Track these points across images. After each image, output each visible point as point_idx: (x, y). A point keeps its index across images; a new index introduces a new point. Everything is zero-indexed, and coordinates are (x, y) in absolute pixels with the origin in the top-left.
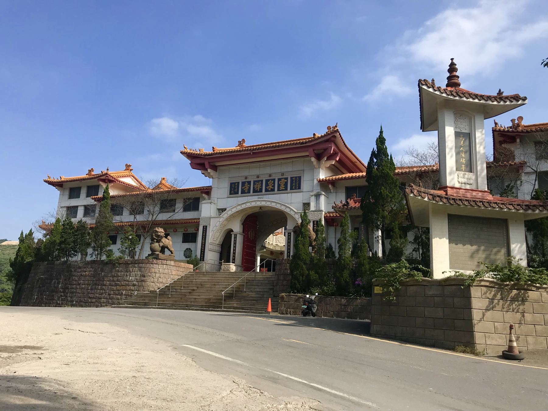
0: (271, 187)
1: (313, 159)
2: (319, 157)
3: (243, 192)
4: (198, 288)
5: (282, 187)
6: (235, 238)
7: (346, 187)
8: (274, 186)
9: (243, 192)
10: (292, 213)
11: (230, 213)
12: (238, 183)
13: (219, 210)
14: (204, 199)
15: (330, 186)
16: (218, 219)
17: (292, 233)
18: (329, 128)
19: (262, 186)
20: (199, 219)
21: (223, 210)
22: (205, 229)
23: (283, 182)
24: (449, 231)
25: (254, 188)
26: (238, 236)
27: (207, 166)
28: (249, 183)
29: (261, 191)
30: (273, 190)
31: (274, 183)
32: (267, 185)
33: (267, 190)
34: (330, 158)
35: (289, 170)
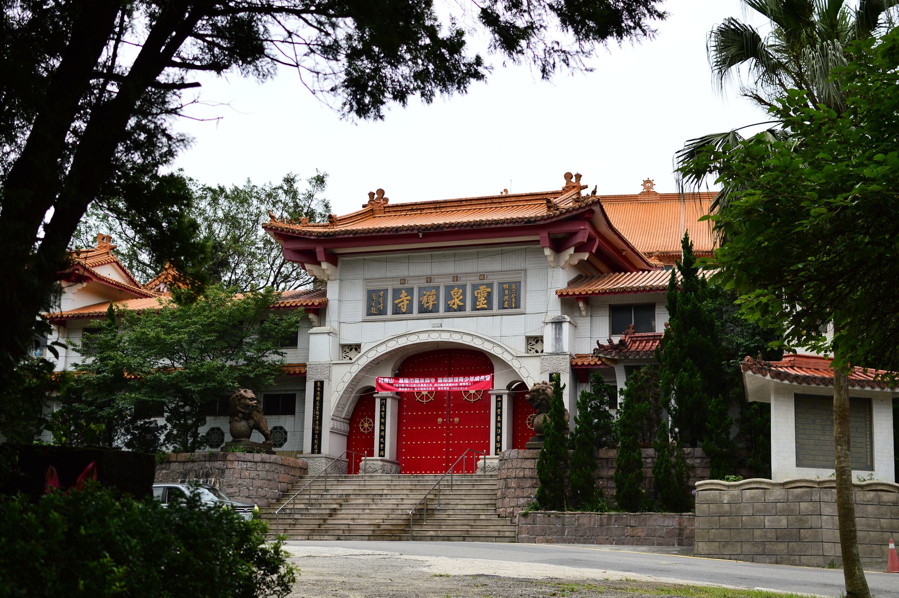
0: (457, 301)
1: (547, 252)
4: (341, 505)
5: (482, 303)
6: (384, 405)
7: (610, 306)
8: (463, 300)
9: (397, 311)
10: (506, 357)
11: (373, 355)
13: (343, 346)
15: (581, 305)
17: (505, 399)
18: (573, 181)
19: (438, 299)
21: (357, 347)
22: (319, 387)
23: (483, 291)
24: (796, 420)
25: (420, 302)
26: (389, 401)
27: (320, 256)
28: (410, 291)
29: (435, 309)
30: (461, 308)
31: (464, 294)
32: (448, 297)
33: (449, 309)
34: (579, 249)
35: (496, 267)
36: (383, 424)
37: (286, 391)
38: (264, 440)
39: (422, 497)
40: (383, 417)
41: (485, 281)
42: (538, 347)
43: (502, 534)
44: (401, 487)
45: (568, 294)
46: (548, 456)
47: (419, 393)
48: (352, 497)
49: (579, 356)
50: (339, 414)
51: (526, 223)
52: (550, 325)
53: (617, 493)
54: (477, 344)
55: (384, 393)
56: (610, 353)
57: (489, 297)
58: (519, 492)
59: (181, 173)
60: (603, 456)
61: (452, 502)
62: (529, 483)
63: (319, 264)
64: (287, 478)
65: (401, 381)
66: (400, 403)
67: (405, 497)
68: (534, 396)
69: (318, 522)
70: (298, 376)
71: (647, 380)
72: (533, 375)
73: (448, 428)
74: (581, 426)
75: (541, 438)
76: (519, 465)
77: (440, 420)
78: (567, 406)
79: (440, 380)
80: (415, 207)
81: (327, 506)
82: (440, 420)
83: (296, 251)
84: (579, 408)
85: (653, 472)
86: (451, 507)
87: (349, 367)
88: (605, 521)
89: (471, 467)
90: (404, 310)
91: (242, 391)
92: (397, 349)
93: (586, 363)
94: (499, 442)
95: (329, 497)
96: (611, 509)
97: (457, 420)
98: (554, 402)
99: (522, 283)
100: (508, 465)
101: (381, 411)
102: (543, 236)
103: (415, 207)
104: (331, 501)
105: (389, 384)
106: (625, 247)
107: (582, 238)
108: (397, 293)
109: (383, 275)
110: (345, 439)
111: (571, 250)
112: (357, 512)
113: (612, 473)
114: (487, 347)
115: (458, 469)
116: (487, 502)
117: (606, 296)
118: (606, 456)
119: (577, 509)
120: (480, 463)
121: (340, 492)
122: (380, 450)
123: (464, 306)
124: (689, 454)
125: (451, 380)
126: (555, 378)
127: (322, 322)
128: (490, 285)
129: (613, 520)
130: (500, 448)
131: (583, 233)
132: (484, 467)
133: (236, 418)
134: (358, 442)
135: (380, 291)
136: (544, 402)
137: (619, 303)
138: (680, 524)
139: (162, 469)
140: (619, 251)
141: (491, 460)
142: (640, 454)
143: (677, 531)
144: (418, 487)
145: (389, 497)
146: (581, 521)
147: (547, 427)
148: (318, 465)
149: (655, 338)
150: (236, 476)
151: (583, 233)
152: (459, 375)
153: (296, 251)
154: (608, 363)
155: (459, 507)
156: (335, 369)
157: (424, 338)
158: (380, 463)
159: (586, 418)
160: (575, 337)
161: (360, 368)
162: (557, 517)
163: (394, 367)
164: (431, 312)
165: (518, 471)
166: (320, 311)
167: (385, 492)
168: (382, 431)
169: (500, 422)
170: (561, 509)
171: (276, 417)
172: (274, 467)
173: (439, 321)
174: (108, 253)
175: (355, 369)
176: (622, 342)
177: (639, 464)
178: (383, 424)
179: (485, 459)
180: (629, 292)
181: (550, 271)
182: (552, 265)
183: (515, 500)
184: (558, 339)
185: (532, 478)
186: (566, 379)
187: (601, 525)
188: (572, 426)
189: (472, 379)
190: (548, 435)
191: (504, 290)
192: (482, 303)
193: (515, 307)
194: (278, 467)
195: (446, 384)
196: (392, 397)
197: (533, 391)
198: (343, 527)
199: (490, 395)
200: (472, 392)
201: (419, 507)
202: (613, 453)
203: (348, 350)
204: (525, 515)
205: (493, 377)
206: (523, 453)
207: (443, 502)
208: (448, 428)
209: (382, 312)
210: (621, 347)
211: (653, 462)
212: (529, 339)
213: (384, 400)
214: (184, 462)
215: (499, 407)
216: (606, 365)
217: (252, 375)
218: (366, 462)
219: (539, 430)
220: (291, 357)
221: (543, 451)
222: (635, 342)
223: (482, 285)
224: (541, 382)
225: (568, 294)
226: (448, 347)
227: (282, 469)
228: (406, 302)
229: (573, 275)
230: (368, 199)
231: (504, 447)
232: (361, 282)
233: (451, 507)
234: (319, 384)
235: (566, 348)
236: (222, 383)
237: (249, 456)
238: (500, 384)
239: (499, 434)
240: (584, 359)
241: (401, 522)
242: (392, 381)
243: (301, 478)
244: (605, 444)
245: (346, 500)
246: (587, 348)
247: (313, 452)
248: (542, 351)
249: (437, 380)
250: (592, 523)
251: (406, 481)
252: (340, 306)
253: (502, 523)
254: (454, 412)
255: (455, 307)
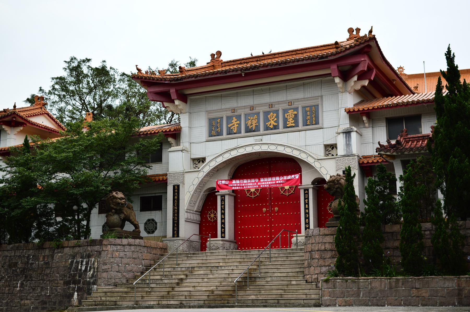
0: (272, 122)
1: (337, 80)
2: (345, 77)
3: (230, 132)
4: (187, 276)
5: (291, 122)
6: (223, 200)
8: (277, 121)
9: (230, 132)
10: (310, 160)
11: (213, 164)
12: (222, 118)
13: (194, 160)
14: (170, 145)
15: (364, 118)
16: (195, 174)
17: (311, 191)
19: (258, 122)
20: (166, 175)
21: (203, 160)
22: (177, 189)
25: (246, 125)
26: (227, 198)
27: (174, 96)
28: (239, 117)
29: (257, 129)
30: (276, 127)
31: (277, 117)
32: (266, 120)
33: (267, 128)
34: (361, 77)
35: (300, 96)
36: (223, 214)
37: (154, 194)
38: (134, 228)
39: (246, 268)
40: (223, 209)
41: (293, 106)
42: (333, 152)
43: (308, 297)
44: (234, 260)
45: (354, 111)
46: (344, 232)
47: (249, 191)
48: (196, 269)
49: (365, 157)
50: (192, 208)
51: (320, 58)
52: (342, 135)
53: (403, 261)
54: (288, 152)
55: (222, 192)
56: (389, 151)
57: (296, 118)
58: (321, 262)
59: (104, 63)
60: (388, 231)
61: (270, 271)
62: (329, 255)
63: (173, 102)
64: (150, 256)
65: (234, 182)
66: (236, 198)
67: (235, 268)
68: (330, 185)
69: (168, 289)
70: (162, 182)
71: (422, 168)
72: (329, 170)
73: (270, 215)
74: (369, 207)
75: (337, 219)
76: (321, 240)
77: (264, 210)
78: (357, 193)
79: (262, 180)
80: (243, 61)
81: (177, 277)
82: (264, 210)
83: (157, 93)
84: (367, 192)
85: (432, 242)
86: (269, 275)
87: (197, 173)
88: (394, 284)
89: (286, 243)
90: (235, 131)
91: (114, 194)
92: (231, 159)
93: (370, 161)
94: (307, 223)
95: (179, 269)
96: (398, 274)
97: (276, 209)
98: (347, 188)
99: (320, 106)
100: (312, 240)
101: (222, 205)
102: (333, 69)
103: (243, 61)
104: (180, 273)
105: (225, 184)
106: (395, 77)
107: (363, 67)
108: (229, 119)
109: (219, 108)
110: (198, 226)
111: (355, 78)
112: (198, 280)
113: (397, 244)
114: (295, 154)
115: (275, 245)
116: (298, 270)
117: (383, 110)
118: (391, 231)
119: (369, 275)
120: (294, 240)
121: (188, 266)
122: (222, 233)
123: (278, 125)
124: (461, 226)
125: (270, 179)
126: (347, 172)
127: (178, 144)
128: (296, 109)
129: (400, 284)
130: (309, 228)
131: (364, 63)
132: (297, 243)
133: (110, 213)
134: (207, 228)
135: (218, 118)
136: (338, 190)
137: (391, 116)
138: (459, 285)
139: (58, 252)
140: (391, 81)
141: (299, 238)
142: (420, 227)
143: (457, 292)
144: (246, 260)
145: (223, 268)
146: (373, 285)
147: (342, 208)
148: (178, 246)
149: (424, 137)
150: (109, 256)
151: (364, 63)
152: (275, 176)
153: (157, 93)
154: (388, 159)
155: (276, 275)
156: (187, 176)
157: (249, 150)
158: (221, 242)
159: (373, 200)
160: (362, 142)
161: (205, 174)
162: (353, 282)
163: (230, 172)
164: (254, 131)
165: (320, 245)
166: (175, 134)
167: (221, 264)
168: (223, 219)
169: (308, 208)
170: (356, 275)
171: (149, 212)
172: (138, 248)
173: (260, 137)
174: (41, 108)
175: (201, 175)
176: (398, 142)
177: (420, 236)
178: (223, 214)
179: (297, 236)
180: (401, 106)
181: (340, 95)
182: (341, 90)
183: (319, 268)
184: (348, 145)
185: (332, 250)
186: (355, 171)
187: (391, 288)
188: (362, 207)
189: (285, 178)
190: (343, 215)
191: (306, 112)
192: (291, 122)
193: (316, 124)
194: (141, 248)
195: (266, 182)
196: (229, 194)
197: (330, 182)
198: (186, 293)
199: (299, 189)
200: (287, 187)
201: (245, 275)
202: (397, 228)
203: (197, 163)
204: (327, 281)
205: (301, 176)
206: (324, 230)
207: (263, 271)
208: (270, 215)
209: (219, 134)
210: (397, 146)
211: (431, 234)
212: (326, 146)
213: (223, 196)
214: (73, 247)
215: (306, 198)
216: (387, 161)
217: (122, 181)
218: (212, 242)
219: (336, 212)
220: (155, 170)
221: (339, 228)
222: (408, 142)
223: (290, 109)
224: (335, 175)
225: (354, 111)
226: (268, 156)
227: (145, 250)
228: (236, 126)
229: (358, 100)
230: (211, 59)
231: (312, 226)
232: (204, 113)
233: (269, 275)
234: (176, 187)
235: (354, 150)
236: (98, 187)
237: (118, 241)
238: (307, 180)
239: (307, 218)
240: (368, 159)
241: (230, 288)
242: (227, 183)
243: (162, 255)
244: (390, 220)
245: (191, 272)
246: (371, 150)
247: (173, 236)
248: (337, 155)
249: (259, 180)
250: (383, 286)
251: (238, 256)
252: (190, 131)
253: (309, 286)
254: (274, 203)
255: (271, 126)
